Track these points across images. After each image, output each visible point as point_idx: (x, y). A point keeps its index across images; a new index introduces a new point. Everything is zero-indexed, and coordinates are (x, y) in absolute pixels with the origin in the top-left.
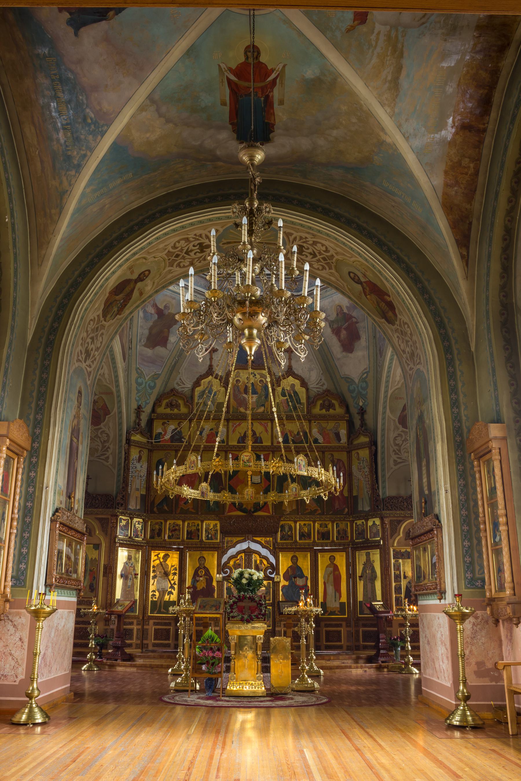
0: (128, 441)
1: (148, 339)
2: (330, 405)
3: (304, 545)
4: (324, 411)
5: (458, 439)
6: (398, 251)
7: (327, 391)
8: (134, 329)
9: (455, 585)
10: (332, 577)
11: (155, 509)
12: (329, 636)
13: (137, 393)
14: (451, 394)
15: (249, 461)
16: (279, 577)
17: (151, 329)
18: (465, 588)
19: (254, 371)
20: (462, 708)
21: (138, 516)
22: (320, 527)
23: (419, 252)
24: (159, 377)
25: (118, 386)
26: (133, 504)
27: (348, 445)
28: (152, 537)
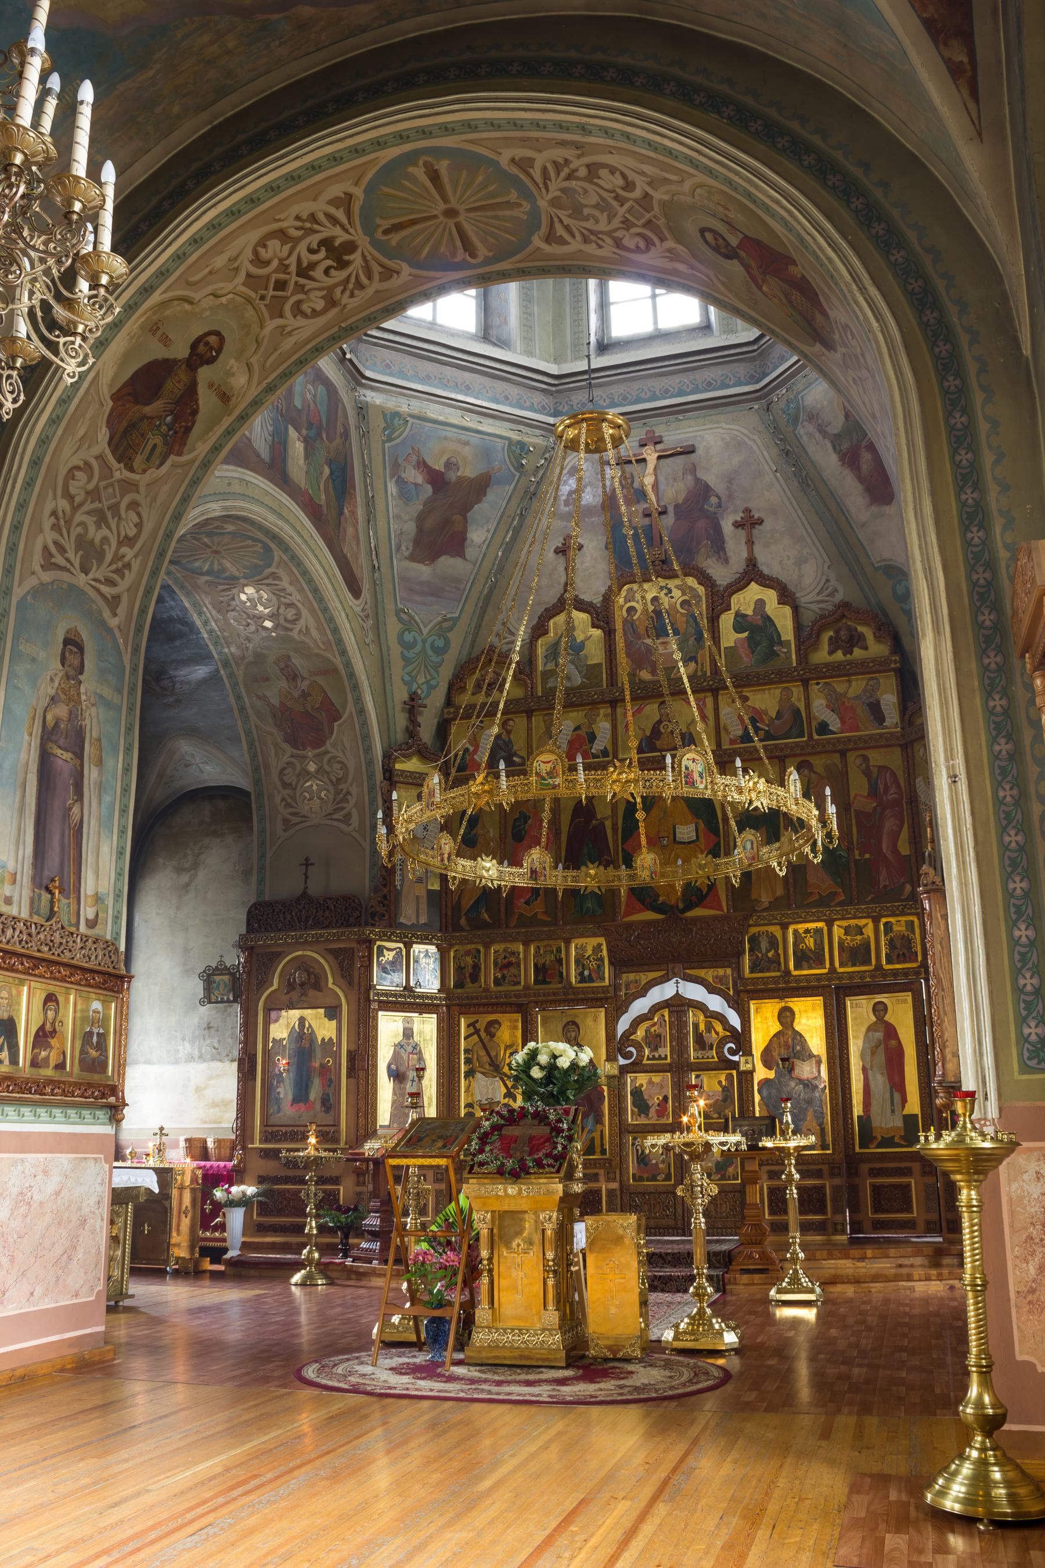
0: (389, 774)
1: (417, 542)
2: (852, 637)
3: (807, 981)
4: (839, 655)
5: (987, 618)
6: (794, 126)
7: (845, 605)
8: (381, 523)
9: (989, 1060)
10: (881, 1057)
11: (463, 922)
12: (883, 1198)
13: (404, 667)
14: (960, 490)
15: (551, 774)
16: (750, 1059)
17: (420, 519)
18: (1022, 1072)
19: (667, 581)
20: (975, 1454)
21: (424, 940)
22: (846, 934)
23: (855, 114)
24: (455, 625)
25: (343, 652)
26: (409, 913)
27: (902, 728)
28: (459, 985)
